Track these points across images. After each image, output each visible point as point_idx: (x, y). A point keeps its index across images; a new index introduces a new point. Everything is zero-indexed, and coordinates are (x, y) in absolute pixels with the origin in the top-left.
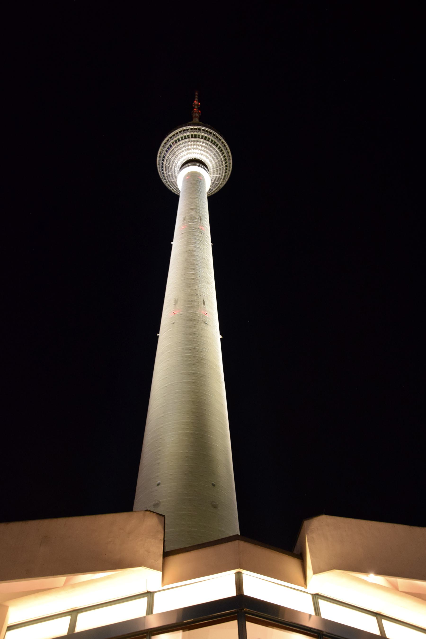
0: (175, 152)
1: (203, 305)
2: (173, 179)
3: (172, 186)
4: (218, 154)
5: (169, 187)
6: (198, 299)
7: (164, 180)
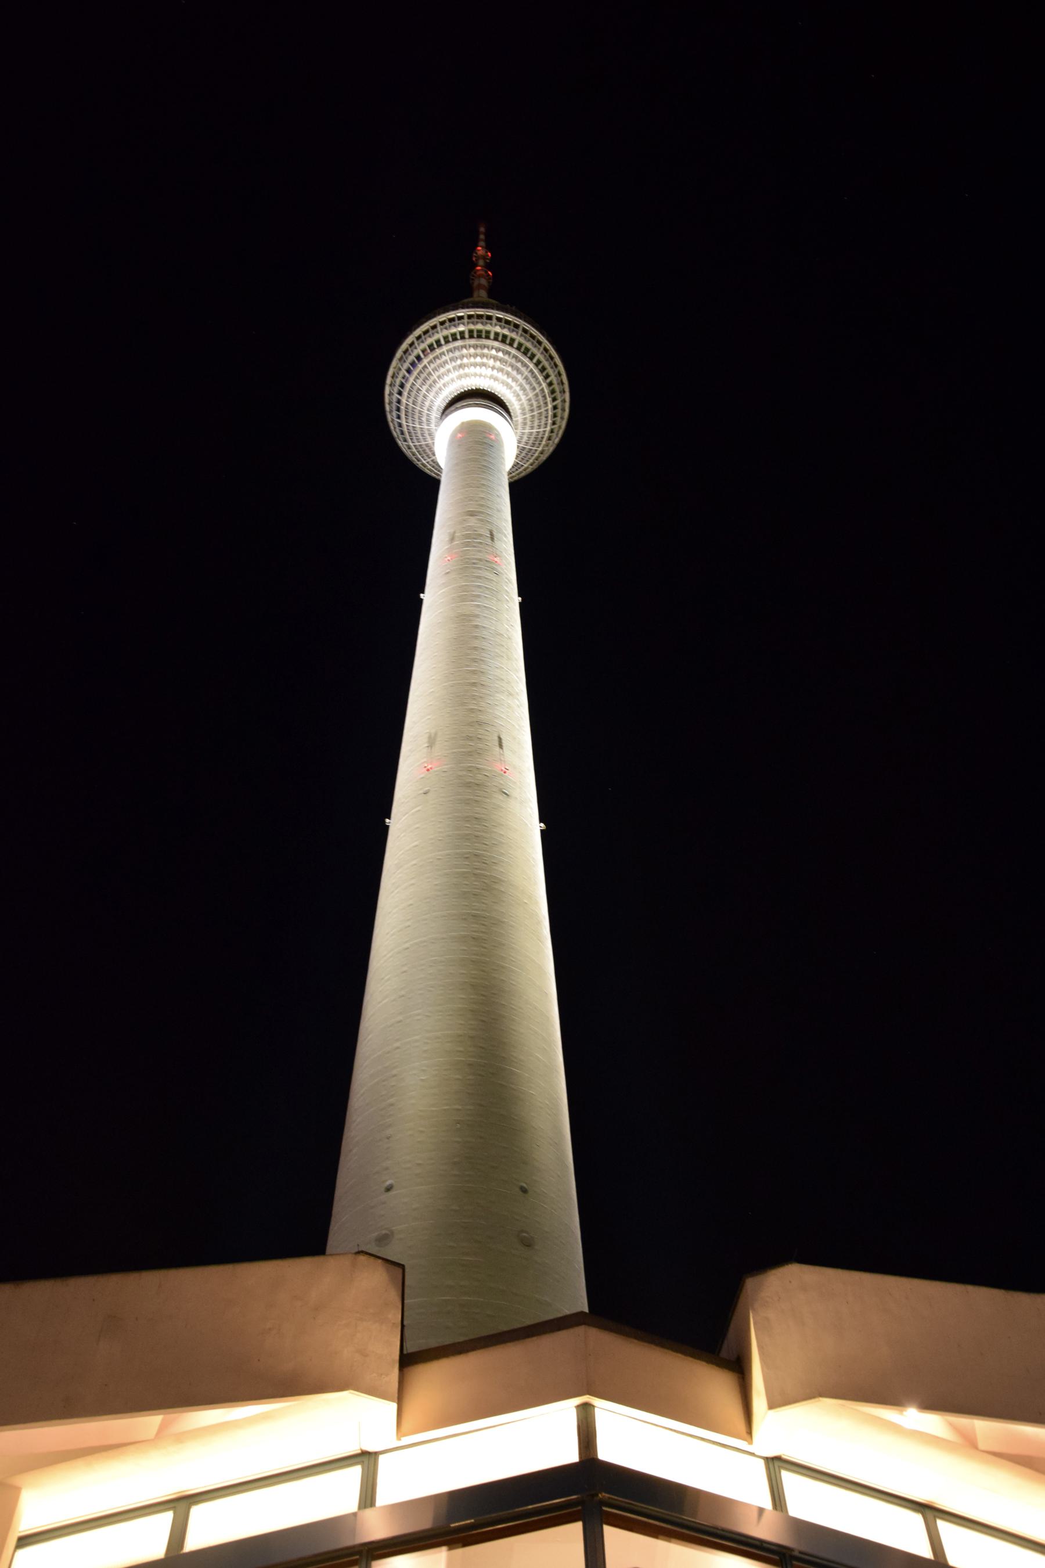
0: (430, 374)
1: (497, 749)
2: (425, 440)
3: (423, 457)
4: (534, 379)
5: (416, 458)
6: (487, 733)
7: (404, 443)
